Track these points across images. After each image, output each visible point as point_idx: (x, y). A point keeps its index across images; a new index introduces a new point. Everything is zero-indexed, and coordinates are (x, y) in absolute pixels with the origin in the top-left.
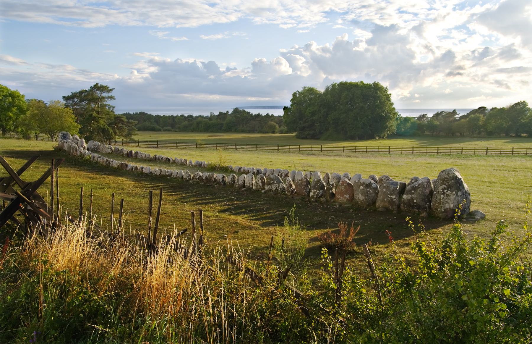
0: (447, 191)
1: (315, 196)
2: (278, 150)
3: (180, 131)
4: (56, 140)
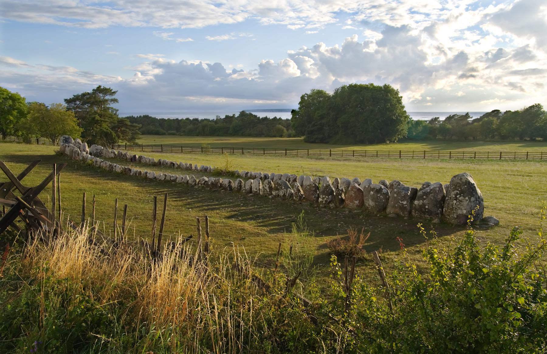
0: (460, 197)
1: (324, 202)
2: (286, 154)
3: (185, 135)
4: (57, 144)
